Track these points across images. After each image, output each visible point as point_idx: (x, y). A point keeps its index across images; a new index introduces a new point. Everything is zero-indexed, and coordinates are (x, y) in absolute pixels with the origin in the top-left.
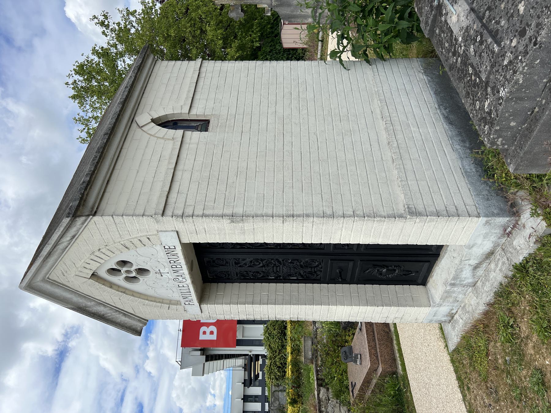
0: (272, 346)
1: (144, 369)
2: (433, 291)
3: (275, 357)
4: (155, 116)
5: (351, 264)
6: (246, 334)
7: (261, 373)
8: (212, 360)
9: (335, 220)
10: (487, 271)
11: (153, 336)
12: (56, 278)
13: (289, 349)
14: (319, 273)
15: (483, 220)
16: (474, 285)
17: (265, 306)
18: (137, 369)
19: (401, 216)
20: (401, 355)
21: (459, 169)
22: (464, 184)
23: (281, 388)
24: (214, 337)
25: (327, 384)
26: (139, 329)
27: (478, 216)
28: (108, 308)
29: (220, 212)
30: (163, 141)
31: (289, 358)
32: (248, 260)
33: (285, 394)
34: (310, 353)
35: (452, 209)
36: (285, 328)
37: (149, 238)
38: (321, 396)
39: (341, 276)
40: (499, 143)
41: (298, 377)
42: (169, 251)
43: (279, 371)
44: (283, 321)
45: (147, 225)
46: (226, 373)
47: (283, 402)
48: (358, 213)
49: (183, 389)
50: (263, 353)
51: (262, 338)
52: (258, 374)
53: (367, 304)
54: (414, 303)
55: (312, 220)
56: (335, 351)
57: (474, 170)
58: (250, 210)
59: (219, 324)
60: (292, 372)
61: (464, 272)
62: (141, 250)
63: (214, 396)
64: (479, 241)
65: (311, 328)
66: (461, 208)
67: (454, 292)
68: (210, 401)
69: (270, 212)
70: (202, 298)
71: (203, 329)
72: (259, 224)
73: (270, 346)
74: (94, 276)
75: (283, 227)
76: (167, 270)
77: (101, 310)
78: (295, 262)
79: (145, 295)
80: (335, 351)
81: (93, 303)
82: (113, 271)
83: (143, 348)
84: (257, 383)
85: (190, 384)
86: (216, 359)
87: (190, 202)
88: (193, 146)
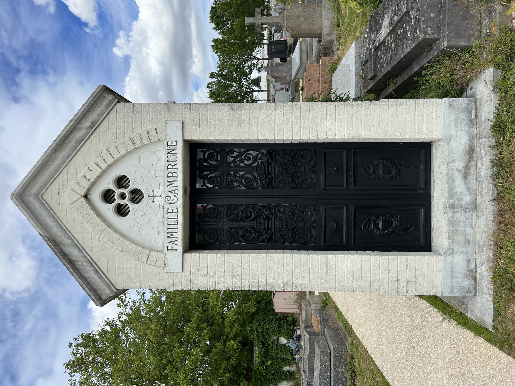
28: (81, 254)
37: (156, 130)
55: (299, 106)
75: (275, 115)
77: (74, 253)
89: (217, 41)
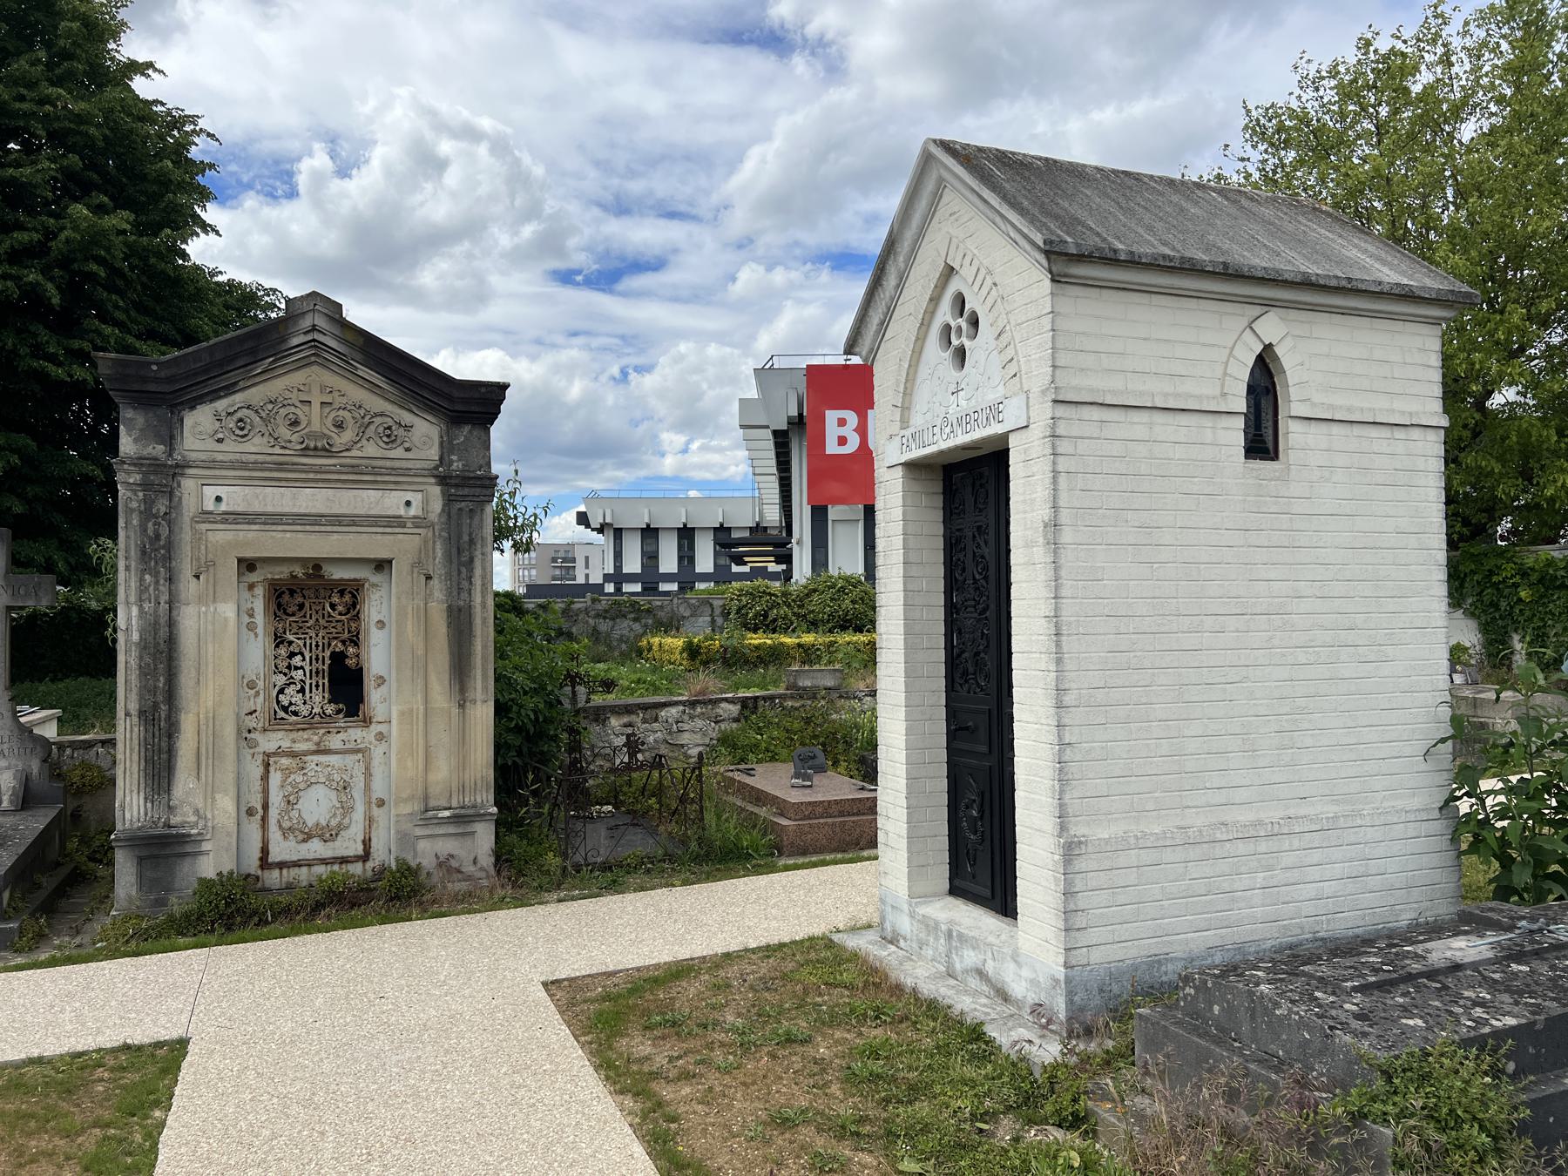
0: (815, 597)
1: (743, 263)
2: (939, 904)
3: (789, 606)
4: (1279, 351)
5: (984, 749)
6: (840, 528)
7: (746, 569)
8: (777, 445)
9: (1053, 711)
10: (976, 993)
11: (825, 276)
12: (945, 199)
13: (808, 638)
14: (966, 687)
15: (1060, 973)
16: (951, 974)
17: (901, 587)
18: (743, 244)
19: (1063, 828)
20: (814, 865)
21: (1165, 950)
22: (1133, 953)
23: (719, 621)
24: (832, 448)
25: (746, 718)
26: (857, 350)
27: (1067, 966)
29: (1061, 503)
30: (1219, 373)
31: (788, 640)
32: (986, 551)
33: (708, 631)
34: (808, 683)
35: (1080, 921)
36: (859, 629)
38: (723, 705)
39: (961, 729)
40: (1188, 990)
41: (747, 662)
42: (995, 411)
43: (757, 615)
44: (873, 622)
45: (1038, 375)
46: (738, 479)
47: (687, 627)
48: (1068, 751)
49: (698, 369)
50: (796, 576)
51: (833, 570)
52: (745, 563)
53: (911, 779)
54: (916, 869)
56: (815, 737)
57: (1164, 979)
58: (1067, 557)
59: (865, 455)
60: (757, 647)
61: (972, 953)
62: (997, 360)
63: (685, 451)
64: (1025, 973)
65: (862, 686)
66: (1082, 939)
67: (937, 938)
68: (672, 439)
69: (1064, 592)
70: (914, 468)
71: (852, 418)
72: (1043, 574)
73: (815, 591)
74: (950, 271)
76: (963, 403)
77: (891, 281)
78: (984, 642)
79: (917, 365)
80: (815, 737)
81: (902, 265)
82: (960, 301)
83: (798, 252)
84: (723, 561)
85: (710, 387)
86: (778, 455)
87: (1083, 446)
88: (1208, 436)
89: (1455, 394)
